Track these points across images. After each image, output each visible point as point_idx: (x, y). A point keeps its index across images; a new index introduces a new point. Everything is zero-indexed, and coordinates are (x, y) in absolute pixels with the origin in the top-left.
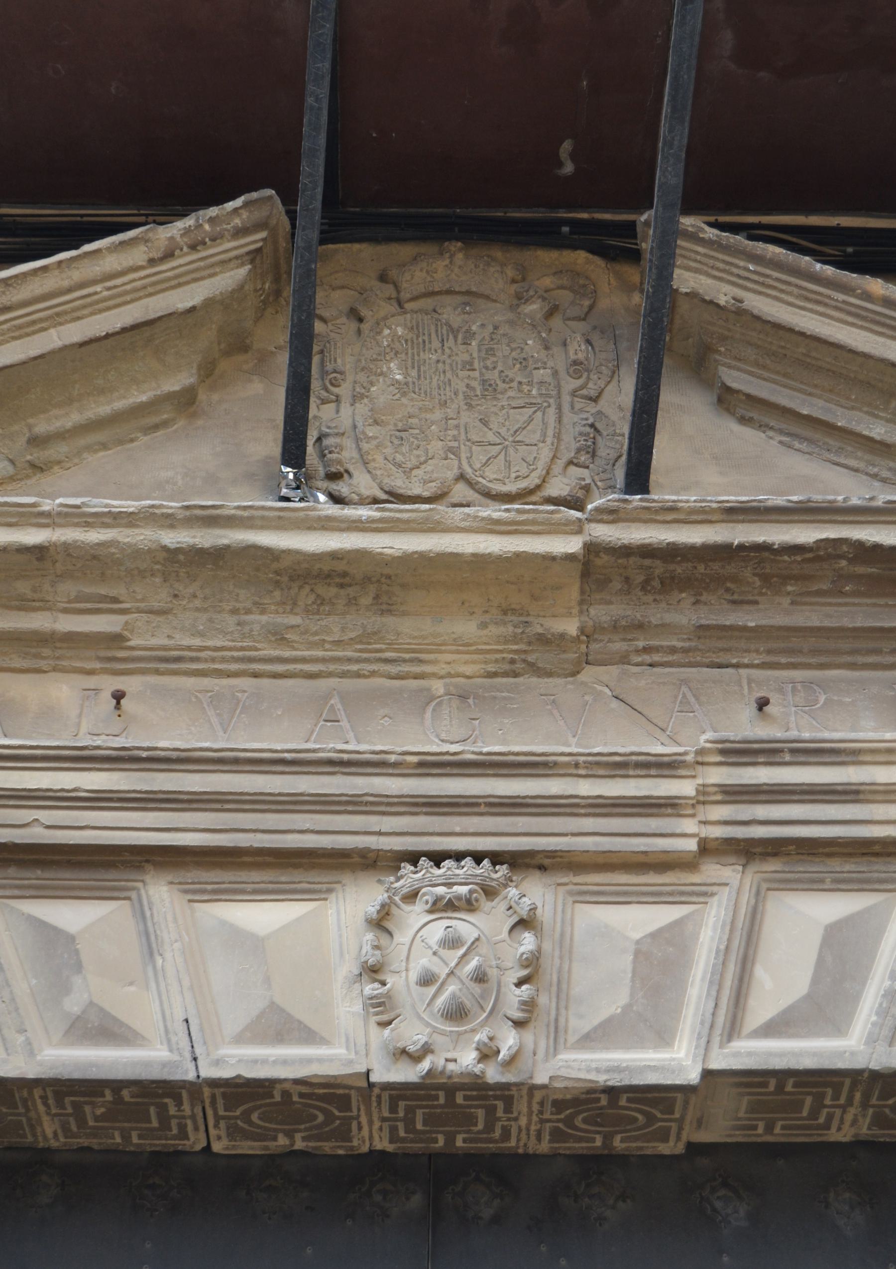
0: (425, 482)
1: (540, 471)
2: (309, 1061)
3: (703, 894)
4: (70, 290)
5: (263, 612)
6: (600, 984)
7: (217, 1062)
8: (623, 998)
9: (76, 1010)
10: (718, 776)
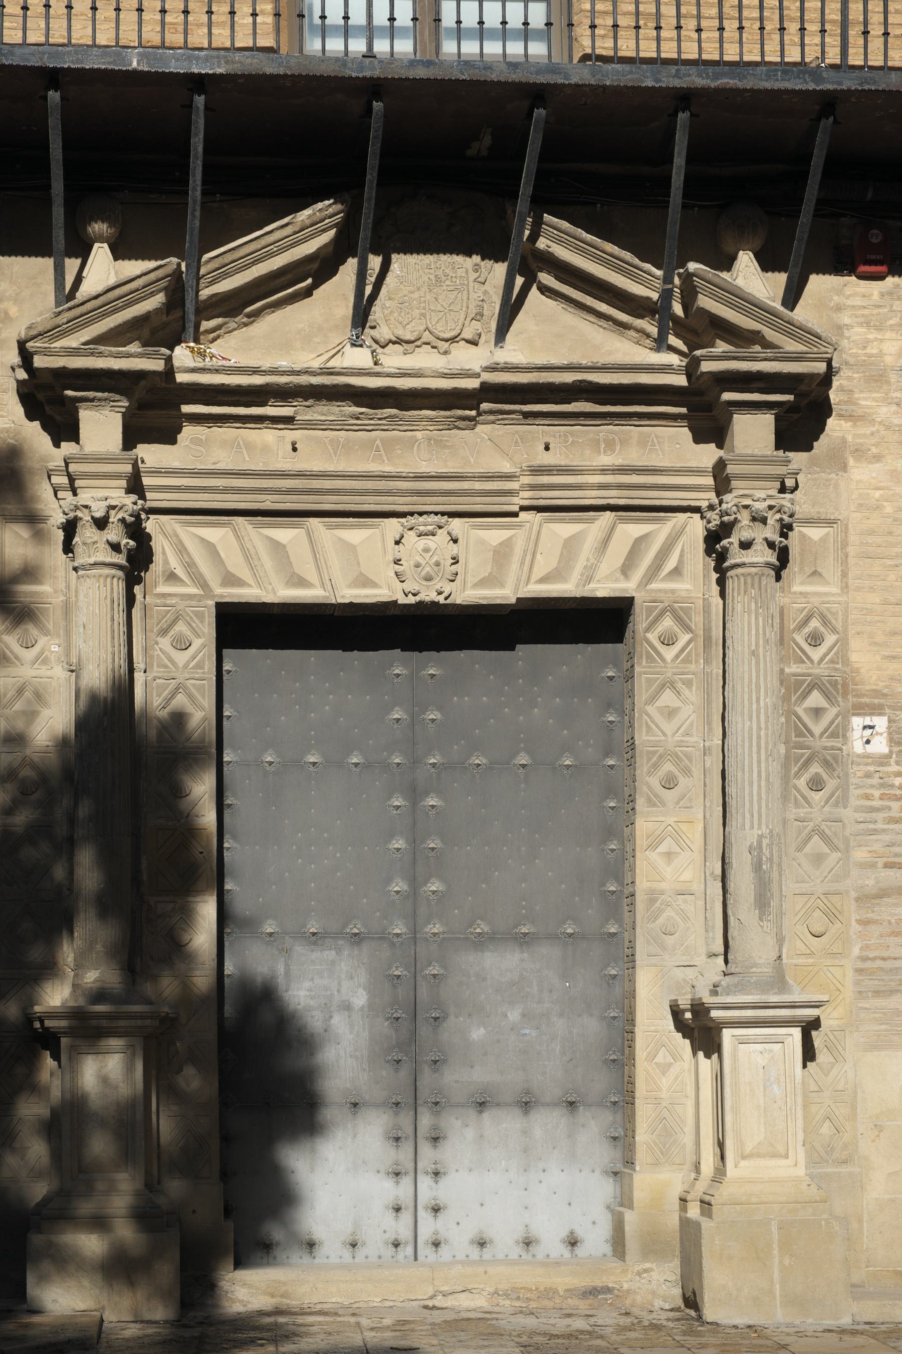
0: (412, 332)
1: (460, 326)
7: (343, 597)
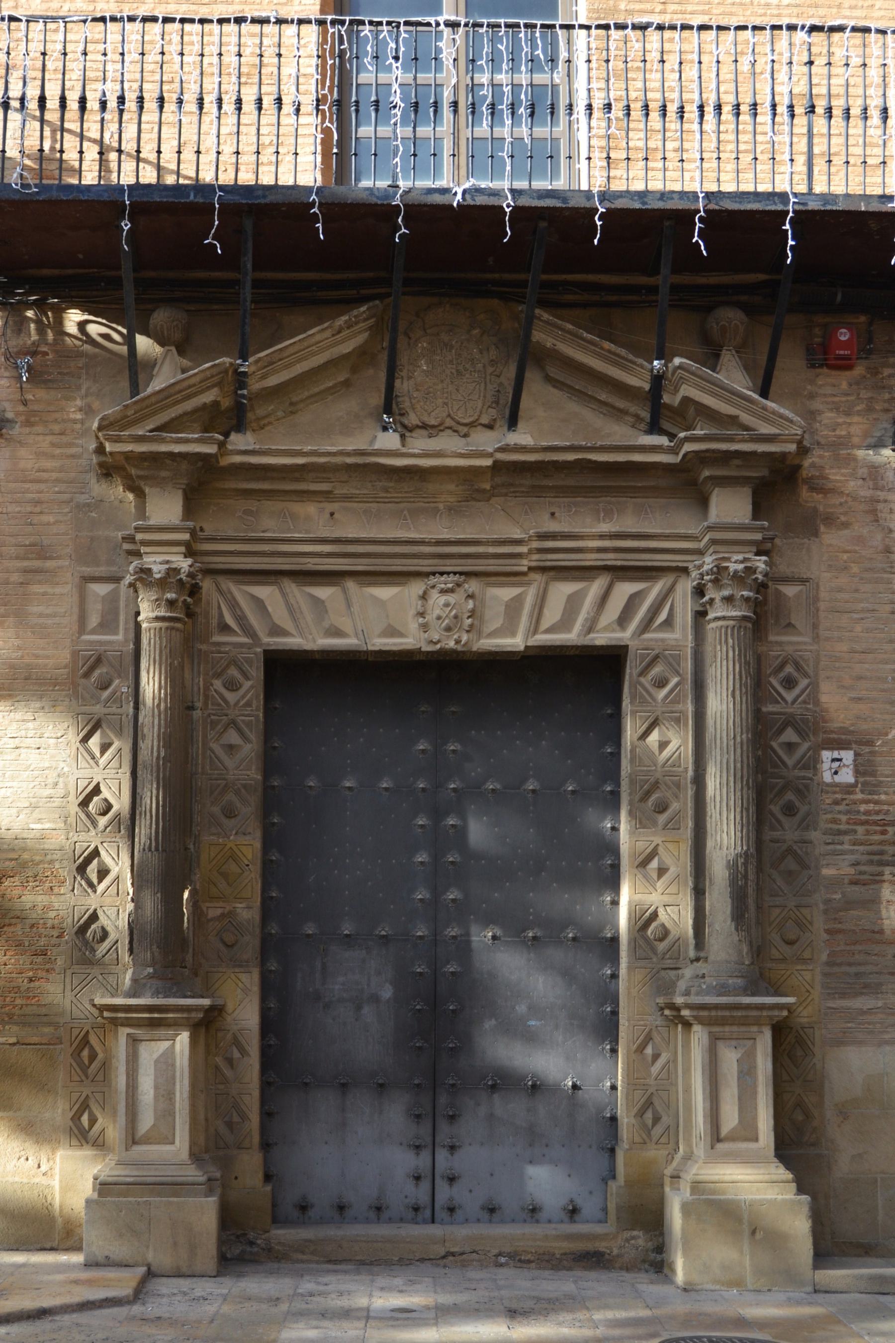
2: (402, 644)
3: (529, 584)
4: (304, 349)
5: (380, 481)
6: (494, 619)
7: (373, 645)
8: (501, 622)
9: (327, 626)
10: (535, 544)
